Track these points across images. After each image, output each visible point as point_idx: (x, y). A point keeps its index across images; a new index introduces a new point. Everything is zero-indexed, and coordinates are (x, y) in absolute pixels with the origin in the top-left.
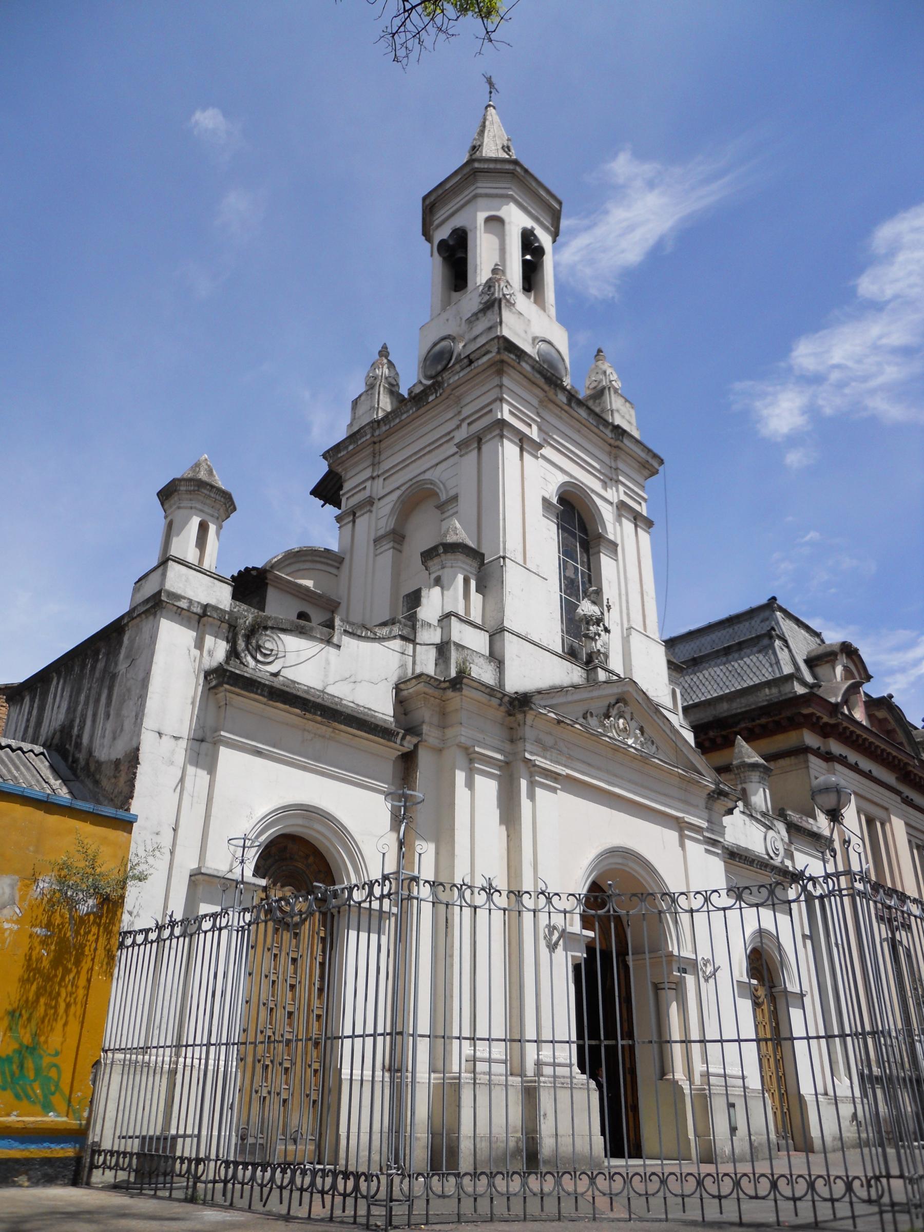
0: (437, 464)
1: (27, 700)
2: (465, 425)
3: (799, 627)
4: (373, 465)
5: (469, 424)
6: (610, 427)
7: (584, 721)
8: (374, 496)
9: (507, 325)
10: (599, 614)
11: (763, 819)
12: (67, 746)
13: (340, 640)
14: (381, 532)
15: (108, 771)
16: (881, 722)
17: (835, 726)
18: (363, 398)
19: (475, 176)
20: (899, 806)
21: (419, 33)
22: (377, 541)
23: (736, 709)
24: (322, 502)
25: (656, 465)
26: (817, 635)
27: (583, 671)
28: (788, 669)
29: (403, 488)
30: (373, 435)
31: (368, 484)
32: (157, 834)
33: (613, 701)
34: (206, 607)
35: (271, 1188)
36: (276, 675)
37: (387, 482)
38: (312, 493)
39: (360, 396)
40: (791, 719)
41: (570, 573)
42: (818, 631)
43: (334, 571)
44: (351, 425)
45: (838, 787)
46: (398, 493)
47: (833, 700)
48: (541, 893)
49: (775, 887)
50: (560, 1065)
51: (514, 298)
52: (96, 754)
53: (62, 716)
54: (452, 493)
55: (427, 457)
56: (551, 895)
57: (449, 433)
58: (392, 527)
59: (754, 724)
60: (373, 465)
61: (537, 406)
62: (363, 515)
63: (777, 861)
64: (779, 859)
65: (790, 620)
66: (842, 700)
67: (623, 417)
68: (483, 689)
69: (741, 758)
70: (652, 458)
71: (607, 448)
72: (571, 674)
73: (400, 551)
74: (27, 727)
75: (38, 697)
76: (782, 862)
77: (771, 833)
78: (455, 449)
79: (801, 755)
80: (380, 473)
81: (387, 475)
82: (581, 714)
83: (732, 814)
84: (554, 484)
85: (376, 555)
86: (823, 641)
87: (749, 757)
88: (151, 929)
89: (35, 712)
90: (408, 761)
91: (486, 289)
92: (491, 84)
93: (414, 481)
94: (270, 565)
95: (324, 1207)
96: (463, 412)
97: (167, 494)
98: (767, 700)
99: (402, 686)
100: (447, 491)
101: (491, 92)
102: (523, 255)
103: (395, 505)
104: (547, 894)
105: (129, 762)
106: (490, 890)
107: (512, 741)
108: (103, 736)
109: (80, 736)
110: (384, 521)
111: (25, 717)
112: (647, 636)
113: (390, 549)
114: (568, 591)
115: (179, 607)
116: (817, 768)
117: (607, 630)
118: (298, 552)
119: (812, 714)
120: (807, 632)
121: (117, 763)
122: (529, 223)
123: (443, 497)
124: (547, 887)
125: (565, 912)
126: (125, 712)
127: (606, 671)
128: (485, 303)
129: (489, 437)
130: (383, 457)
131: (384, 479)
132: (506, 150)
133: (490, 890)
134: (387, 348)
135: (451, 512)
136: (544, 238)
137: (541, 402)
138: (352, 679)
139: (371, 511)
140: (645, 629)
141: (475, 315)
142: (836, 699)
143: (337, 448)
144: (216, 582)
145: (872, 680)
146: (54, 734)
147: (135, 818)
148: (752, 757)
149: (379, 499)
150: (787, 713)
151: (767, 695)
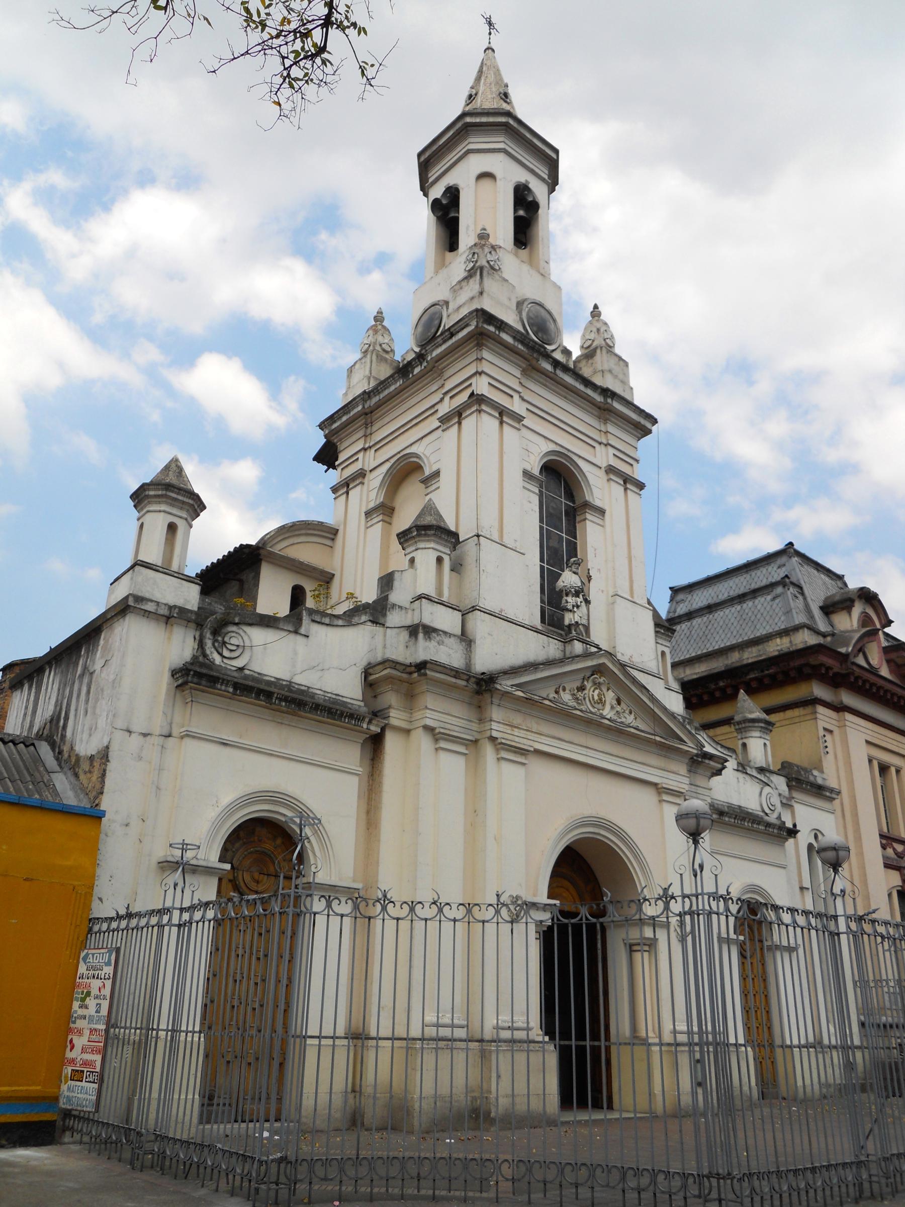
0: (422, 438)
1: (26, 687)
2: (447, 399)
3: (818, 570)
4: (365, 436)
5: (451, 398)
6: (599, 390)
7: (556, 696)
8: (366, 468)
9: (489, 295)
10: (579, 584)
11: (759, 776)
14: (372, 505)
15: (85, 766)
17: (848, 675)
18: (357, 366)
19: (467, 131)
21: (300, 88)
22: (368, 514)
23: (748, 658)
24: (325, 467)
26: (840, 578)
27: (560, 643)
28: (800, 618)
29: (393, 461)
30: (364, 407)
31: (360, 455)
32: (127, 825)
34: (171, 608)
35: (191, 1164)
36: (241, 669)
38: (314, 459)
39: (355, 363)
40: (799, 670)
41: (554, 543)
42: (839, 572)
43: (328, 542)
44: (346, 394)
45: (697, 813)
46: (387, 465)
47: (843, 650)
48: (433, 903)
49: (643, 902)
50: (518, 1029)
51: (499, 263)
52: (77, 748)
53: (51, 707)
54: (434, 468)
55: (414, 429)
56: (442, 905)
57: (433, 406)
58: (382, 500)
59: (762, 674)
60: (365, 436)
61: (519, 377)
62: (355, 486)
63: (772, 818)
64: (775, 815)
65: (808, 565)
66: (852, 650)
67: (616, 377)
68: (448, 672)
69: (741, 713)
70: (645, 419)
71: (596, 412)
72: (550, 648)
73: (390, 524)
74: (25, 715)
75: (34, 686)
76: (779, 818)
77: (767, 790)
78: (438, 424)
79: (810, 706)
80: (371, 444)
81: (378, 446)
83: (721, 775)
85: (368, 528)
86: (845, 585)
87: (751, 712)
88: (113, 918)
89: (32, 698)
90: (375, 743)
91: (470, 256)
92: (490, 24)
93: (402, 454)
94: (263, 542)
95: (228, 1183)
96: (445, 386)
97: (140, 497)
98: (778, 650)
99: (371, 671)
100: (431, 466)
101: (490, 34)
102: (515, 211)
103: (384, 477)
104: (439, 904)
105: (101, 759)
106: (384, 901)
107: (481, 720)
108: (83, 731)
109: (65, 727)
110: (373, 495)
111: (24, 705)
112: (634, 602)
113: (379, 522)
114: (551, 561)
115: (146, 611)
118: (291, 527)
119: (822, 665)
121: (92, 758)
122: (523, 176)
123: (427, 472)
124: (439, 898)
125: (455, 920)
126: (98, 711)
127: (583, 642)
128: (469, 271)
129: (468, 412)
130: (375, 428)
131: (375, 451)
132: (503, 97)
133: (384, 901)
134: (382, 313)
136: (539, 190)
137: (524, 372)
138: (320, 668)
139: (363, 484)
140: (632, 597)
141: (460, 282)
142: (847, 649)
143: (332, 419)
144: (184, 582)
145: (892, 624)
146: (46, 724)
147: (103, 813)
148: (753, 712)
149: (371, 471)
150: (797, 663)
151: (778, 645)
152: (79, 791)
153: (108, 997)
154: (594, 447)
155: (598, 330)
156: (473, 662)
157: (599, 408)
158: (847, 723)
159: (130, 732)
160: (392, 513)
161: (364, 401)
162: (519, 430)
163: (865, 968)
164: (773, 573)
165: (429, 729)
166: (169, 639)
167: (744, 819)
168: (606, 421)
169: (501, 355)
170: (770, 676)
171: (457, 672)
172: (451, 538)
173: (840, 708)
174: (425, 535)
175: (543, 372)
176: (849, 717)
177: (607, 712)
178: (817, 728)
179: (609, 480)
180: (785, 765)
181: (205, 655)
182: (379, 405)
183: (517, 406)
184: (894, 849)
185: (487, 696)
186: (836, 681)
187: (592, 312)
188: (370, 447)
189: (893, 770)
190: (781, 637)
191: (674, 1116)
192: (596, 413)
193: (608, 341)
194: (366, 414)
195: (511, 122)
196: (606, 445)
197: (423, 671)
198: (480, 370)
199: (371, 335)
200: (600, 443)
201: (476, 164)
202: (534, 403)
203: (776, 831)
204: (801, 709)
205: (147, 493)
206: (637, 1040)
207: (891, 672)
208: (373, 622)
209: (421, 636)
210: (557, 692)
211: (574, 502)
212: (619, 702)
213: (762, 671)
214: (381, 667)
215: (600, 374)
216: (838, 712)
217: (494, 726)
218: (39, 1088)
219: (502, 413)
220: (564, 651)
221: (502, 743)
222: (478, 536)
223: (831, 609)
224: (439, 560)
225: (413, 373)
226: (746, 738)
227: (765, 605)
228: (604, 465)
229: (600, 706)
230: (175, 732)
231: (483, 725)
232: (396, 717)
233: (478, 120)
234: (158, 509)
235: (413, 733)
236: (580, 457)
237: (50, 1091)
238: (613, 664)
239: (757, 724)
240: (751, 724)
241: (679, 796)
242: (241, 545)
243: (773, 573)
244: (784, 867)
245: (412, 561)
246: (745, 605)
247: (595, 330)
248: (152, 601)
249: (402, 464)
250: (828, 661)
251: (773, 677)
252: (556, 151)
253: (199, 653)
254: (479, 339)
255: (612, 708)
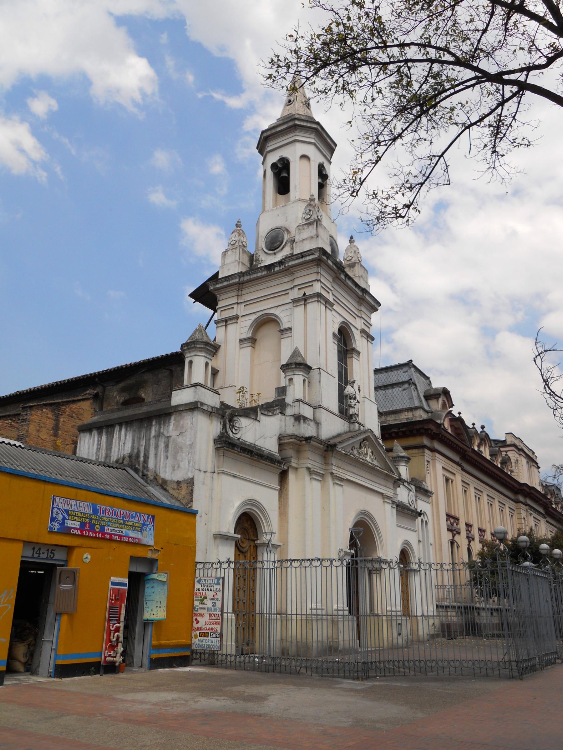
2: (296, 289)
3: (420, 375)
12: (137, 466)
13: (260, 418)
16: (458, 434)
17: (438, 434)
19: (295, 128)
20: (460, 472)
24: (194, 300)
25: (376, 306)
30: (240, 280)
31: (235, 306)
33: (362, 440)
36: (239, 439)
37: (246, 307)
42: (428, 375)
47: (439, 422)
55: (272, 300)
63: (412, 508)
71: (358, 300)
73: (254, 348)
81: (247, 303)
82: (350, 449)
84: (337, 324)
85: (240, 348)
87: (401, 453)
99: (282, 438)
107: (326, 464)
116: (428, 456)
117: (358, 402)
119: (429, 429)
120: (424, 378)
129: (311, 300)
130: (244, 292)
135: (287, 335)
137: (333, 280)
138: (264, 437)
139: (237, 323)
142: (441, 422)
150: (418, 427)
152: (170, 498)
153: (221, 599)
154: (356, 318)
155: (355, 252)
156: (320, 434)
157: (359, 298)
158: (436, 458)
159: (200, 471)
160: (255, 342)
161: (240, 277)
162: (332, 311)
163: (449, 578)
164: (400, 375)
165: (308, 469)
166: (211, 423)
167: (404, 508)
168: (360, 304)
169: (326, 271)
170: (402, 431)
171: (322, 441)
172: (308, 368)
173: (433, 450)
174: (299, 368)
175: (340, 280)
176: (437, 455)
177: (368, 459)
178: (424, 460)
179: (362, 336)
180: (413, 479)
181: (227, 432)
182: (248, 281)
183: (330, 298)
184: (450, 521)
185: (330, 453)
186: (433, 437)
187: (350, 240)
188: (241, 303)
189: (450, 481)
190: (408, 412)
191: (392, 649)
192: (357, 300)
193: (359, 258)
194: (240, 284)
195: (319, 128)
196: (360, 317)
197: (309, 441)
198: (318, 279)
199: (237, 236)
200: (358, 316)
201: (301, 149)
202: (336, 295)
203: (410, 512)
204: (417, 450)
205: (196, 345)
206: (373, 614)
207: (452, 431)
208: (280, 413)
209: (302, 421)
210: (352, 450)
211: (346, 347)
212: (372, 453)
213: (399, 429)
214: (289, 437)
215: (358, 278)
216: (432, 452)
217: (334, 468)
218: (184, 641)
219: (327, 302)
220: (350, 427)
221: (336, 476)
222: (319, 369)
223: (429, 398)
224: (304, 380)
225: (274, 270)
226: (398, 465)
227: (398, 393)
228: (359, 328)
229: (366, 456)
230: (216, 472)
231: (326, 466)
232: (294, 463)
233: (302, 123)
234: (201, 354)
235: (300, 470)
236: (351, 324)
237: (188, 642)
238: (372, 435)
239: (404, 459)
240: (401, 459)
241: (390, 499)
242: (177, 352)
243: (401, 376)
244: (415, 531)
245: (291, 380)
246: (387, 391)
247: (353, 252)
248: (206, 404)
249: (264, 318)
250: (432, 427)
251: (404, 432)
252: (336, 145)
253: (224, 431)
254: (318, 262)
255: (370, 457)
